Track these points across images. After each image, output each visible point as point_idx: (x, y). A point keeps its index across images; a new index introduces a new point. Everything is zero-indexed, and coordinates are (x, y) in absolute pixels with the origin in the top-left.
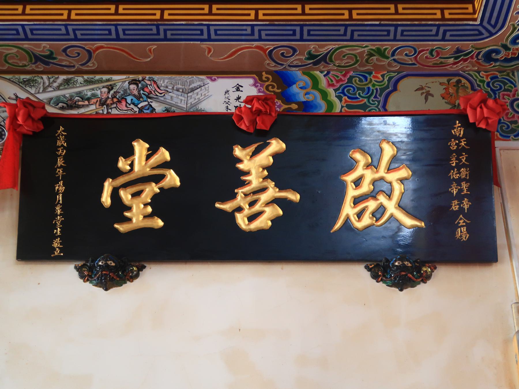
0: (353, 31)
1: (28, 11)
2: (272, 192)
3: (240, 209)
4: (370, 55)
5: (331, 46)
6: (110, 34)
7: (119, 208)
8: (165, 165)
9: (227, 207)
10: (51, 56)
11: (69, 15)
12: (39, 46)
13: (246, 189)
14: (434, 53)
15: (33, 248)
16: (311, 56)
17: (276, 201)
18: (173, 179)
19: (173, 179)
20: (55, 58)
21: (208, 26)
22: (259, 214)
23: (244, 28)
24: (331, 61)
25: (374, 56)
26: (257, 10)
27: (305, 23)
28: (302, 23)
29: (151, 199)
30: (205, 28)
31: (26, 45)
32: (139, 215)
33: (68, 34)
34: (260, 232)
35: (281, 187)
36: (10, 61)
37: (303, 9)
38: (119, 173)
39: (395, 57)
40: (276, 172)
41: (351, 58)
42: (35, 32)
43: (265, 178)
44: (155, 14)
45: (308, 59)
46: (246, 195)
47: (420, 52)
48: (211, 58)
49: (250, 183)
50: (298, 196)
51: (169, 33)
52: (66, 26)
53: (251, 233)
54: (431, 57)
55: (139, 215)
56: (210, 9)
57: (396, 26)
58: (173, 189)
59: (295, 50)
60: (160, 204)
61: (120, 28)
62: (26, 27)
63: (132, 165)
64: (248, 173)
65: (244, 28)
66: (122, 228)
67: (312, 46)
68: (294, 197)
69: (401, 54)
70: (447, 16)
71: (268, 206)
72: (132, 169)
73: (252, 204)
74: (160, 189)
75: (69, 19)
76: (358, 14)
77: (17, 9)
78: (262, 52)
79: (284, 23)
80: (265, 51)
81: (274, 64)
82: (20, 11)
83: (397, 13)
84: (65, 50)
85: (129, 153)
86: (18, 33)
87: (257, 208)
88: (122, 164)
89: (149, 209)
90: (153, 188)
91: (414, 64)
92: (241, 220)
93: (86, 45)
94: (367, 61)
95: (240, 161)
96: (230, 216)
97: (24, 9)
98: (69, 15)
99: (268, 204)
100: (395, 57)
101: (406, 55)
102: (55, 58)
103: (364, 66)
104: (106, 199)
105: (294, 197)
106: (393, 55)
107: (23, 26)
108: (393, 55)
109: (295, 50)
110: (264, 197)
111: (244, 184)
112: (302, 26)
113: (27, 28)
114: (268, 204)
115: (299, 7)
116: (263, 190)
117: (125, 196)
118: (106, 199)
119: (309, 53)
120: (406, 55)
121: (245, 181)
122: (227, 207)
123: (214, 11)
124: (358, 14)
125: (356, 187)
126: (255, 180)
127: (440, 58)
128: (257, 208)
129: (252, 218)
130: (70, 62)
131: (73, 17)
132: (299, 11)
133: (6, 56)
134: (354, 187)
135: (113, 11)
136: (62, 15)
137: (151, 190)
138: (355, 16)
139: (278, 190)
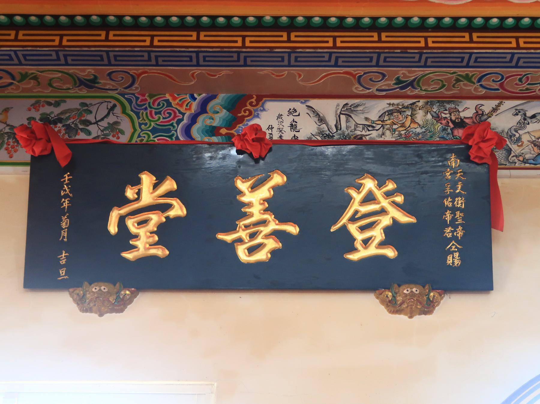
0: (329, 60)
1: (20, 37)
2: (273, 226)
3: (240, 241)
4: (458, 80)
5: (419, 72)
6: (102, 60)
7: (125, 238)
8: (169, 194)
9: (229, 238)
10: (94, 80)
11: (152, 41)
12: (84, 71)
13: (247, 221)
14: (524, 80)
15: (40, 272)
16: (399, 81)
17: (277, 234)
18: (178, 210)
19: (178, 210)
20: (98, 83)
21: (107, 52)
22: (260, 246)
23: (323, 55)
24: (419, 86)
25: (462, 81)
26: (517, 38)
27: (200, 50)
28: (381, 51)
29: (157, 228)
30: (194, 55)
31: (72, 70)
32: (144, 244)
33: (58, 59)
34: (259, 264)
35: (281, 219)
36: (55, 85)
37: (289, 36)
38: (127, 201)
39: (483, 83)
40: (276, 206)
41: (439, 84)
42: (28, 58)
43: (266, 210)
44: (145, 41)
45: (396, 84)
46: (247, 227)
47: (507, 78)
48: (300, 83)
49: (251, 215)
50: (298, 229)
51: (160, 60)
52: (57, 52)
53: (249, 265)
54: (520, 83)
55: (144, 244)
56: (107, 35)
57: (471, 54)
58: (178, 219)
59: (384, 76)
60: (166, 233)
61: (111, 54)
62: (18, 52)
63: (139, 193)
64: (249, 205)
65: (323, 55)
66: (129, 256)
67: (402, 72)
68: (293, 229)
69: (488, 80)
70: (339, 44)
71: (269, 238)
72: (138, 199)
73: (253, 236)
74: (167, 218)
75: (152, 45)
76: (342, 42)
77: (100, 35)
78: (351, 77)
79: (461, 51)
80: (354, 76)
81: (362, 88)
82: (12, 37)
83: (471, 41)
84: (110, 74)
85: (138, 182)
86: (11, 59)
87: (259, 240)
88: (130, 193)
89: (156, 238)
90: (155, 218)
91: (498, 90)
92: (242, 253)
93: (131, 70)
94: (454, 86)
95: (241, 193)
96: (231, 247)
97: (17, 35)
98: (152, 41)
99: (267, 236)
100: (483, 83)
101: (493, 81)
102: (98, 83)
103: (451, 90)
104: (113, 229)
105: (293, 229)
106: (479, 81)
107: (15, 52)
108: (479, 81)
109: (384, 76)
110: (266, 230)
111: (246, 215)
112: (197, 53)
113: (20, 54)
114: (267, 236)
115: (194, 34)
116: (264, 223)
117: (131, 224)
118: (113, 229)
119: (398, 79)
120: (493, 81)
121: (246, 213)
122: (229, 238)
123: (202, 38)
124: (525, 43)
125: (249, 253)
126: (256, 212)
127: (529, 84)
128: (259, 240)
129: (252, 250)
130: (113, 86)
131: (156, 43)
132: (285, 38)
133: (51, 80)
134: (247, 254)
135: (103, 37)
136: (53, 41)
137: (155, 218)
138: (339, 44)
139: (277, 222)
